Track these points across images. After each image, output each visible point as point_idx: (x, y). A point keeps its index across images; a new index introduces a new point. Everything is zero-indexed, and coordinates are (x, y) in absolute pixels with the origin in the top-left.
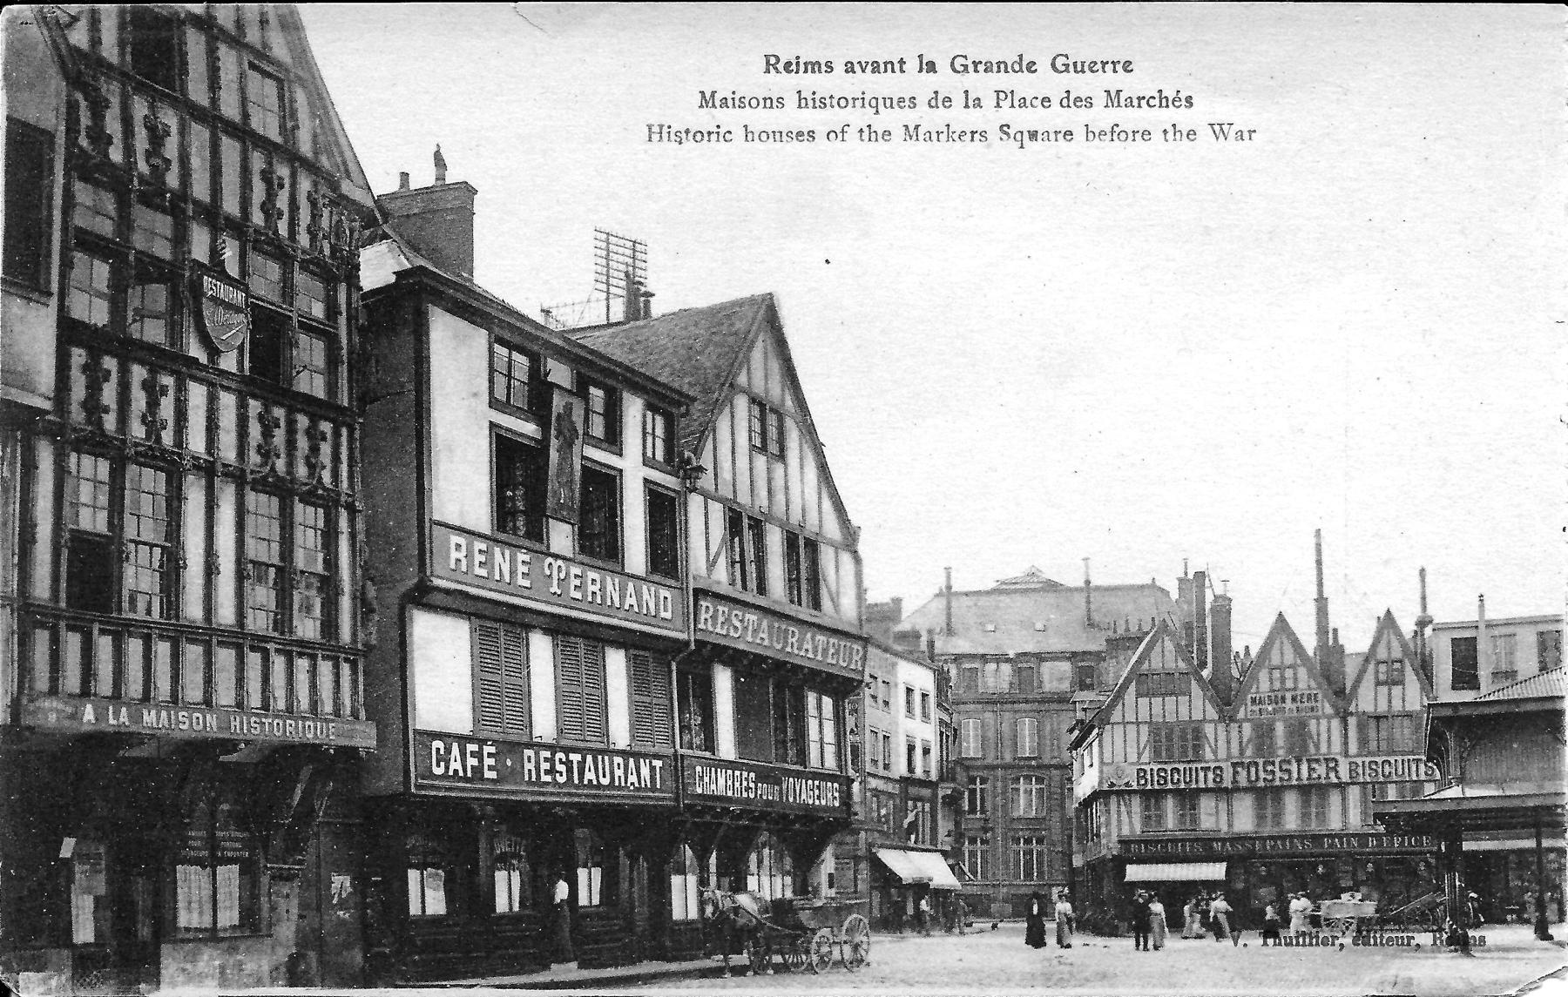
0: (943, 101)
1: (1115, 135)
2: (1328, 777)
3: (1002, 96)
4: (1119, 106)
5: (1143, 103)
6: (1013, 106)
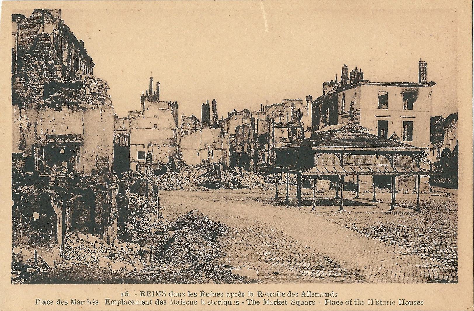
0: (160, 302)
3: (38, 301)
4: (268, 304)
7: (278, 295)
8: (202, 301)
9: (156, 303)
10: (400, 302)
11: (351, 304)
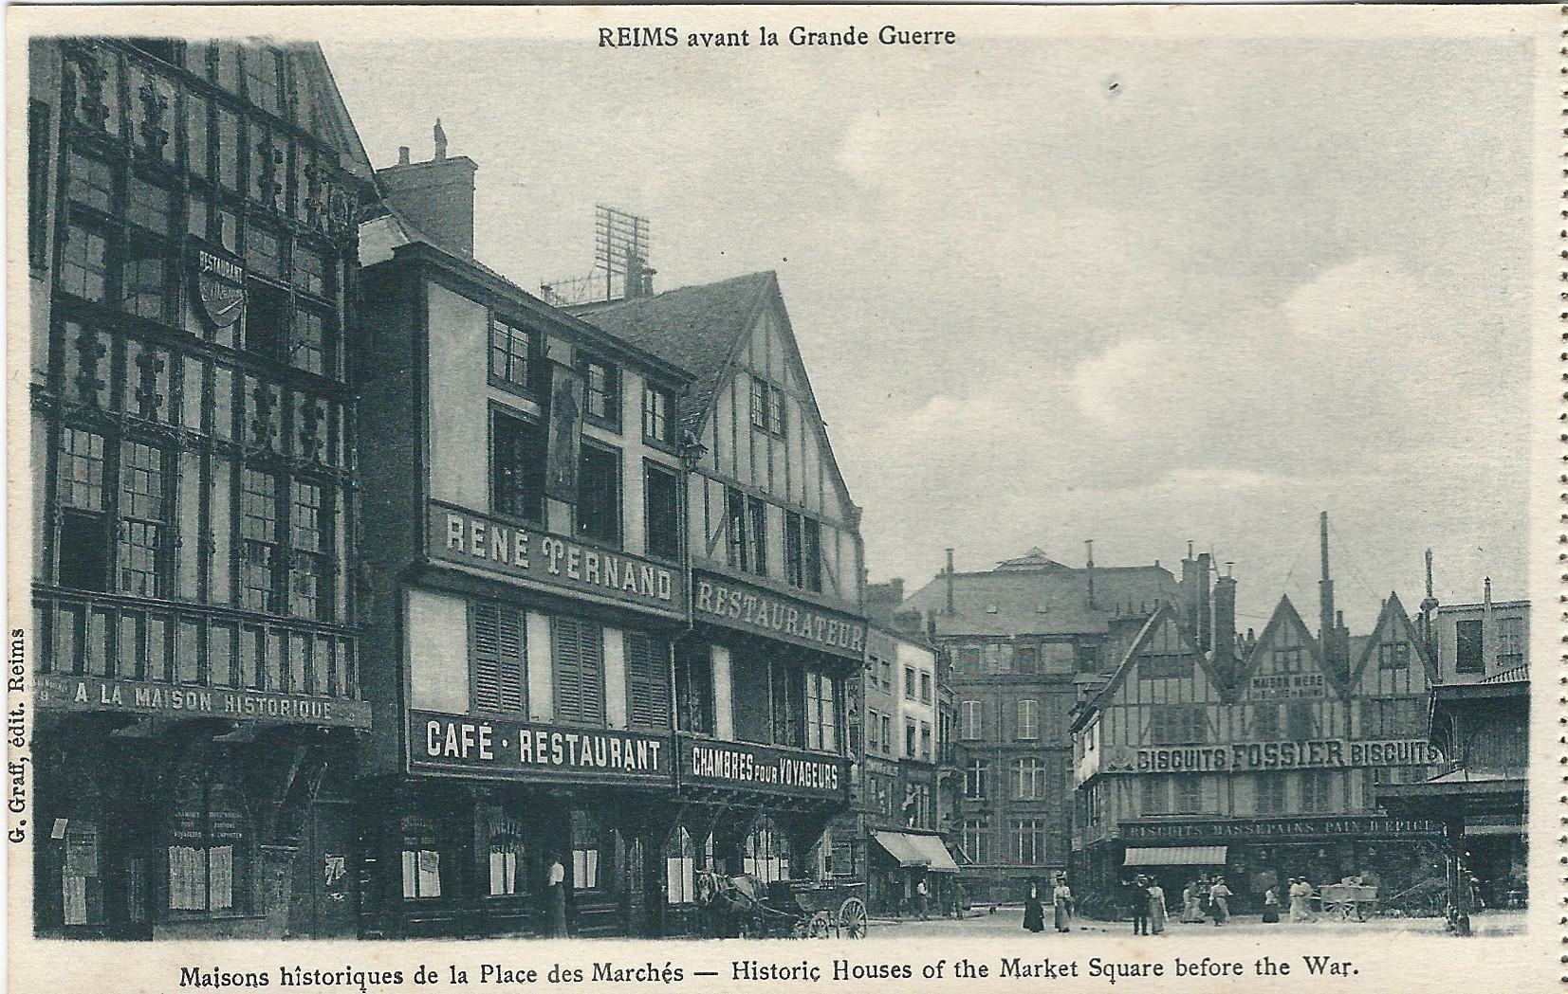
0: (430, 976)
2: (1330, 761)
3: (487, 970)
5: (633, 975)
6: (499, 982)
7: (18, 720)
8: (284, 975)
9: (924, 973)
10: (736, 970)
11: (940, 977)
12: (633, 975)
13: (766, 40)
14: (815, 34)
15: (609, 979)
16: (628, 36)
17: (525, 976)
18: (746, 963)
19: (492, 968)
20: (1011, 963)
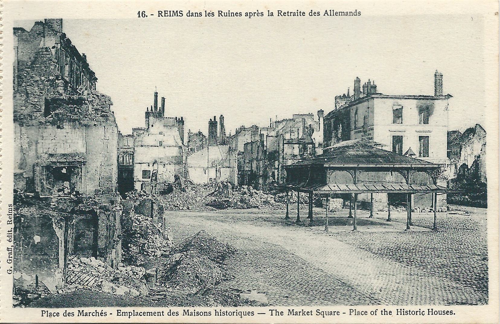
1: (411, 312)
3: (44, 312)
5: (91, 314)
6: (355, 315)
10: (398, 312)
11: (376, 315)
12: (91, 314)
13: (270, 15)
14: (292, 12)
15: (188, 315)
16: (167, 13)
17: (142, 314)
18: (401, 310)
19: (353, 310)
20: (291, 311)
